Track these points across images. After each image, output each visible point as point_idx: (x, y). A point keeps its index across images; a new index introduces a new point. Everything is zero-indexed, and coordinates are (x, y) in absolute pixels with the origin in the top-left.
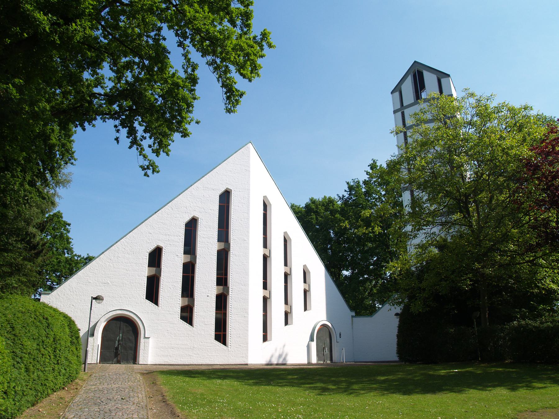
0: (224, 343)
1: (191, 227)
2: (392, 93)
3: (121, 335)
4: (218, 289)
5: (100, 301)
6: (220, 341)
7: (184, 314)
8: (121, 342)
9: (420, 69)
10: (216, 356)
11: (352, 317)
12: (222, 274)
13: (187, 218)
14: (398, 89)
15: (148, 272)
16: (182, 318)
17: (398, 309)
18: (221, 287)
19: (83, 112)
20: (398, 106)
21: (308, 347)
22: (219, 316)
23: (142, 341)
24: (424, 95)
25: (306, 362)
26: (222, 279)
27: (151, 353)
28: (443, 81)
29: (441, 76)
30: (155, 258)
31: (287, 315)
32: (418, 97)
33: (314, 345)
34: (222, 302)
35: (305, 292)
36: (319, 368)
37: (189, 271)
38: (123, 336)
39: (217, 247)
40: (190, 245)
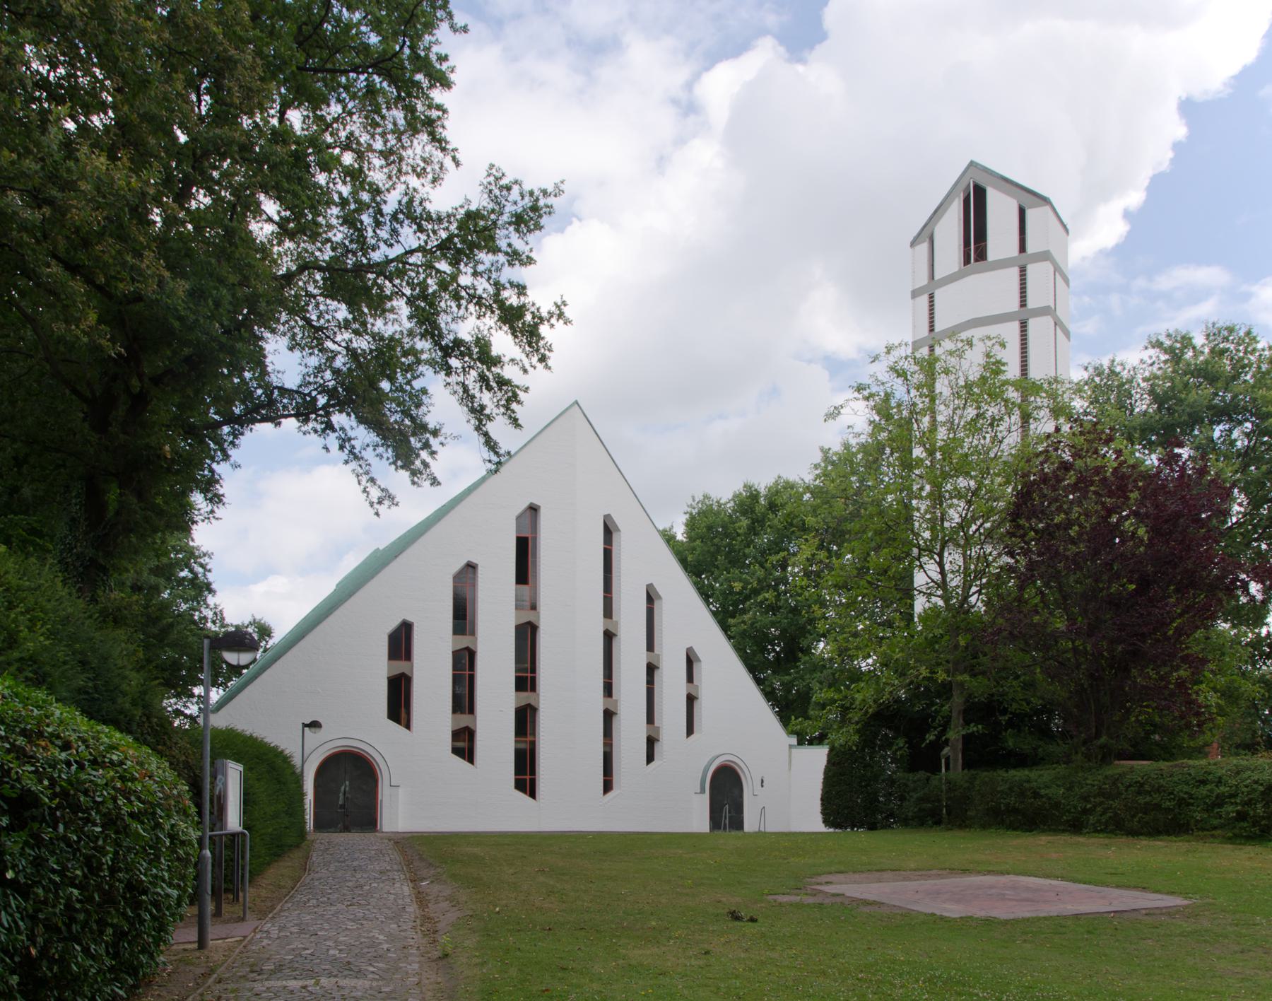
0: (533, 795)
2: (913, 244)
4: (517, 698)
6: (398, 721)
7: (460, 744)
9: (982, 183)
11: (791, 746)
12: (525, 670)
14: (926, 235)
15: (454, 643)
16: (456, 751)
18: (459, 716)
20: (923, 280)
22: (522, 746)
26: (526, 681)
27: (401, 812)
29: (1029, 200)
31: (651, 742)
34: (525, 720)
35: (691, 699)
37: (464, 663)
40: (463, 616)
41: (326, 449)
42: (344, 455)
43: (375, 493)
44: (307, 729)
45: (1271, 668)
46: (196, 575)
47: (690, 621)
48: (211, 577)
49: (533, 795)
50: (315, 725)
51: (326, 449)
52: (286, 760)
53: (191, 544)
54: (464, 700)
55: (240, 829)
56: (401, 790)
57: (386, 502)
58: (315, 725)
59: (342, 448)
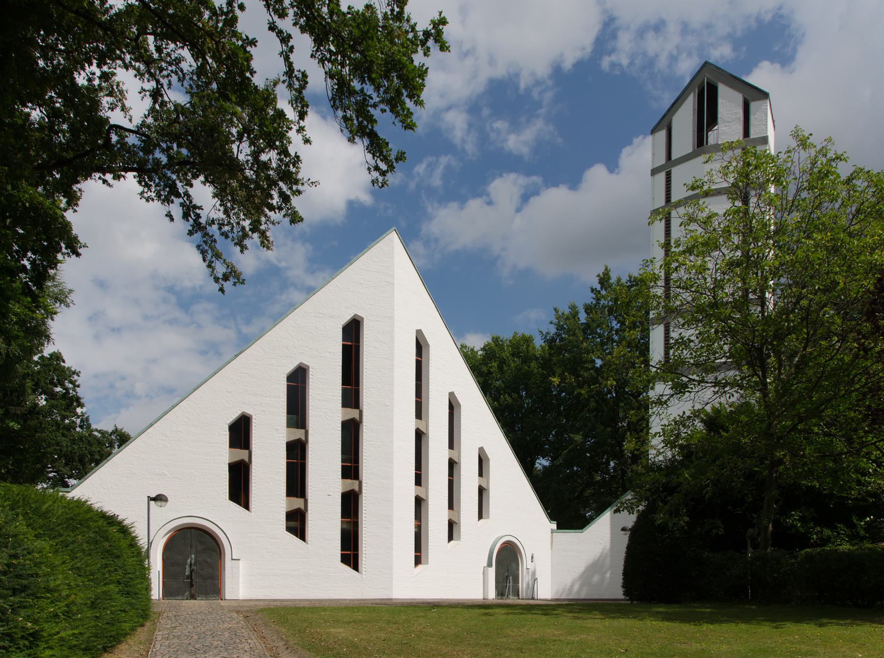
0: (356, 567)
1: (298, 380)
3: (193, 556)
4: (343, 484)
5: (163, 503)
8: (193, 567)
9: (714, 80)
10: (338, 585)
13: (291, 367)
15: (343, 415)
16: (289, 529)
17: (629, 519)
18: (349, 481)
19: (94, 150)
20: (662, 160)
21: (485, 574)
22: (345, 526)
23: (228, 563)
24: (712, 138)
25: (481, 597)
26: (351, 468)
28: (753, 106)
30: (240, 432)
31: (451, 525)
32: (701, 141)
33: (492, 571)
34: (350, 504)
35: (482, 491)
36: (148, 589)
37: (297, 453)
38: (197, 555)
39: (340, 415)
41: (169, 216)
42: (187, 226)
43: (220, 269)
44: (152, 503)
45: (2, 644)
46: (67, 389)
47: (482, 428)
48: (80, 392)
49: (356, 567)
50: (159, 498)
51: (169, 216)
52: (124, 530)
53: (63, 364)
54: (296, 483)
55: (623, 597)
56: (241, 563)
57: (232, 280)
58: (159, 498)
59: (186, 216)
